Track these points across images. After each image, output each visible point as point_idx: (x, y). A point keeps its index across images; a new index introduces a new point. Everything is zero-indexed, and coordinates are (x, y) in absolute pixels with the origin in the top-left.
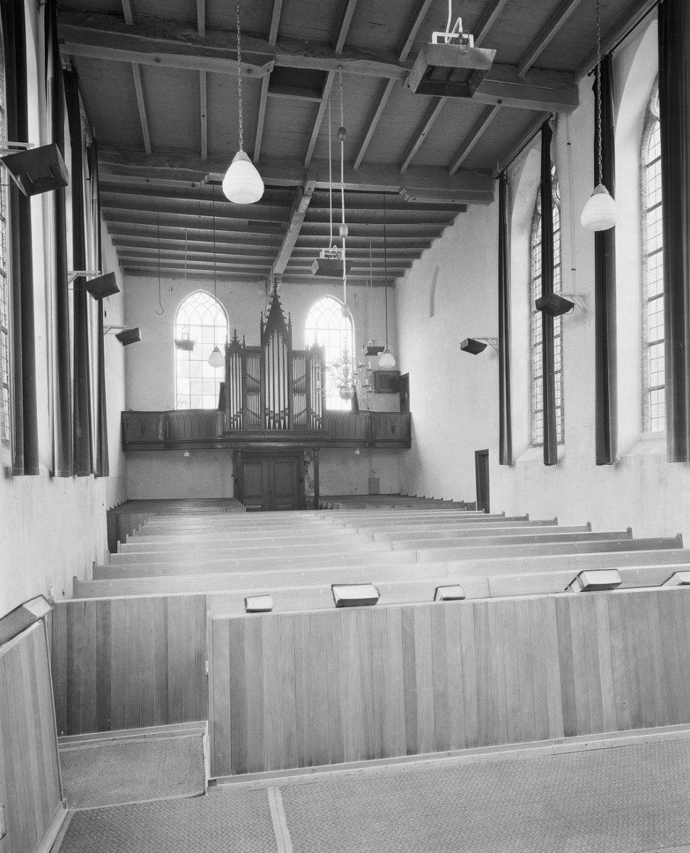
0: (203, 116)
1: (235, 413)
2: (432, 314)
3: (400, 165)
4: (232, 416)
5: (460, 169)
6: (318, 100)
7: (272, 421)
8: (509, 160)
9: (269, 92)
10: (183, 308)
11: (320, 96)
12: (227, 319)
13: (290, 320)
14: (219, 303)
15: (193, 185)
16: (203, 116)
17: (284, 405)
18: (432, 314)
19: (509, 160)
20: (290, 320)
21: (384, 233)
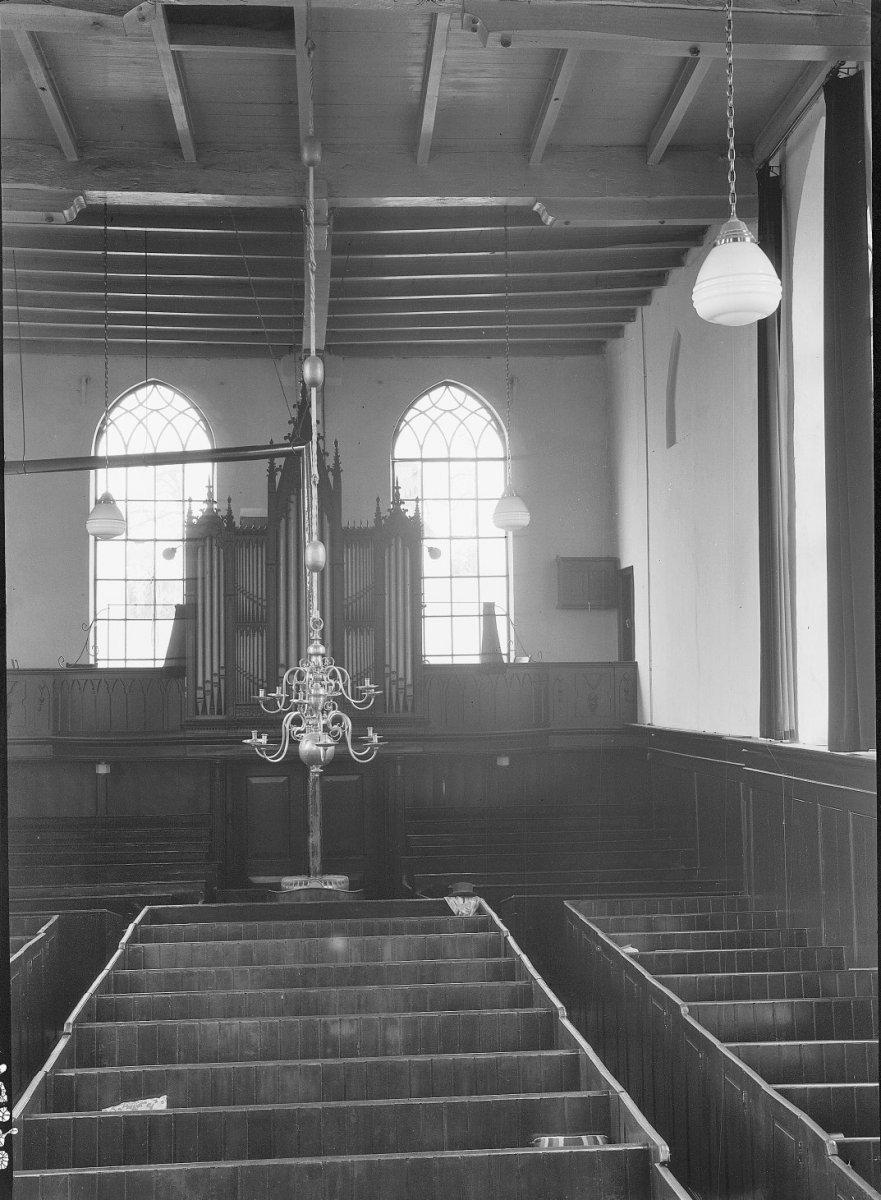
0: (43, 89)
1: (208, 677)
2: (671, 441)
3: (526, 146)
4: (200, 684)
5: (673, 148)
6: (291, 53)
7: (394, 687)
8: (792, 116)
9: (171, 43)
10: (407, 423)
11: (290, 42)
12: (503, 439)
13: (337, 458)
14: (487, 408)
15: (50, 219)
16: (43, 89)
17: (212, 669)
18: (671, 441)
19: (792, 116)
20: (337, 458)
21: (147, 304)
